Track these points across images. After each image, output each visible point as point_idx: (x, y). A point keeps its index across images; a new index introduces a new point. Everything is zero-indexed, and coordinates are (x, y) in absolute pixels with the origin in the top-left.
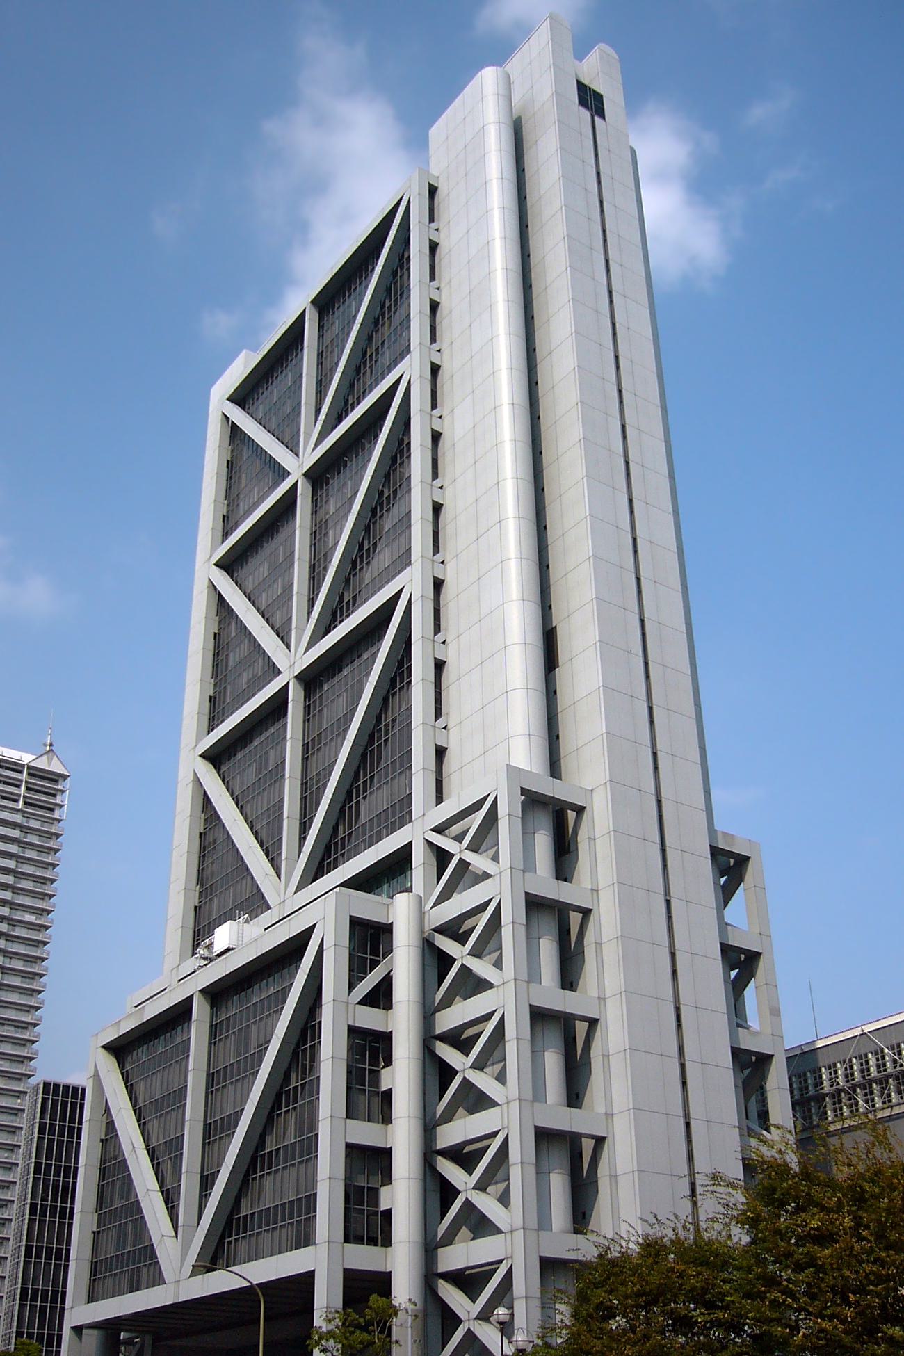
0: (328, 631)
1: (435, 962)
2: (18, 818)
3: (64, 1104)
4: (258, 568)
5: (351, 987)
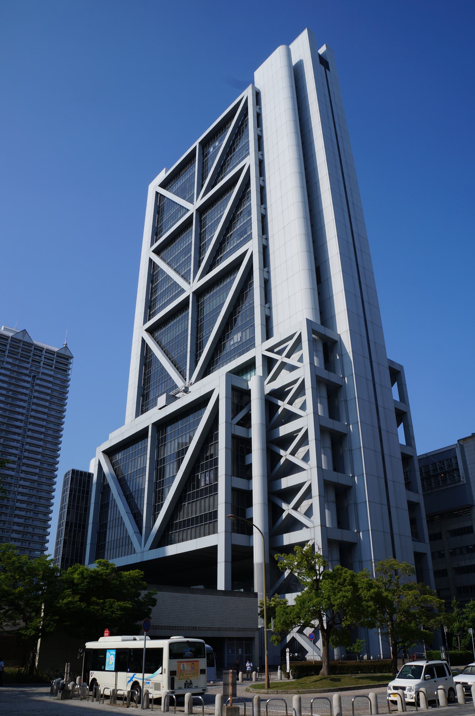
2: (52, 373)
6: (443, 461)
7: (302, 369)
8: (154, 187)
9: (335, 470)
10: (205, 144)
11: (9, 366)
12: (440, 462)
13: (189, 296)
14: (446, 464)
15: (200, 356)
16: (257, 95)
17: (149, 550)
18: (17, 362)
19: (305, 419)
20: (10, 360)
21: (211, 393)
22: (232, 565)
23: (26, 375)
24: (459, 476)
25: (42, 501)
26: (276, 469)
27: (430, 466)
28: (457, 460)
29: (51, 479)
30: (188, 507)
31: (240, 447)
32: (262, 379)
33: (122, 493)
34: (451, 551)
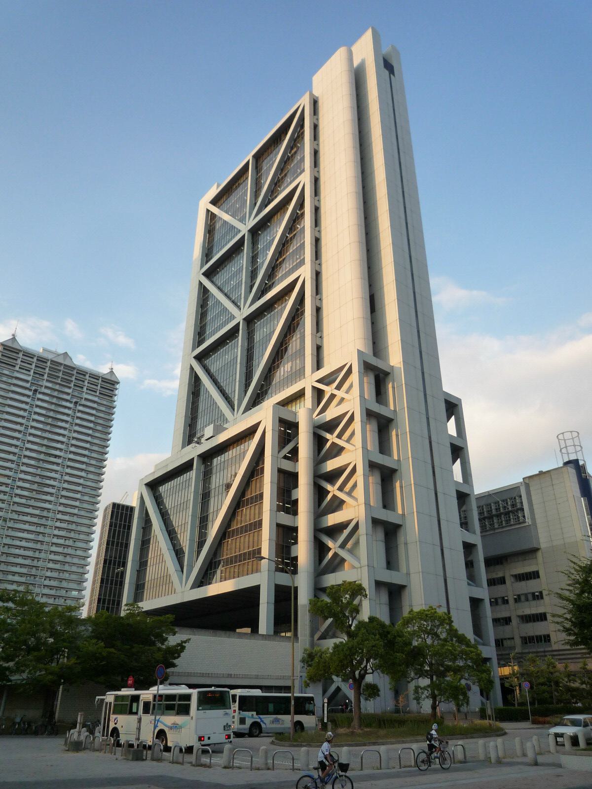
0: (259, 299)
1: (319, 441)
2: (96, 399)
3: (122, 514)
4: (223, 276)
5: (279, 452)
6: (507, 500)
7: (350, 400)
8: (204, 204)
9: (385, 507)
10: (259, 157)
11: (48, 391)
12: (503, 501)
13: (239, 322)
14: (509, 503)
15: (249, 386)
16: (315, 103)
17: (190, 589)
18: (57, 387)
19: (353, 453)
20: (50, 385)
21: (258, 424)
22: (275, 606)
23: (67, 401)
24: (524, 517)
25: (82, 537)
26: (323, 503)
27: (492, 504)
28: (521, 500)
29: (91, 512)
30: (232, 543)
31: (287, 481)
32: (312, 411)
33: (164, 528)
34: (515, 597)
